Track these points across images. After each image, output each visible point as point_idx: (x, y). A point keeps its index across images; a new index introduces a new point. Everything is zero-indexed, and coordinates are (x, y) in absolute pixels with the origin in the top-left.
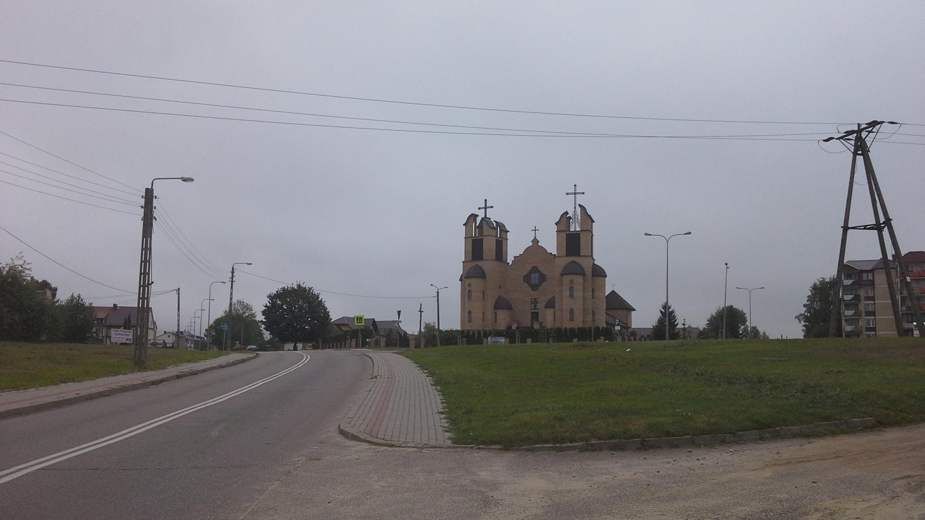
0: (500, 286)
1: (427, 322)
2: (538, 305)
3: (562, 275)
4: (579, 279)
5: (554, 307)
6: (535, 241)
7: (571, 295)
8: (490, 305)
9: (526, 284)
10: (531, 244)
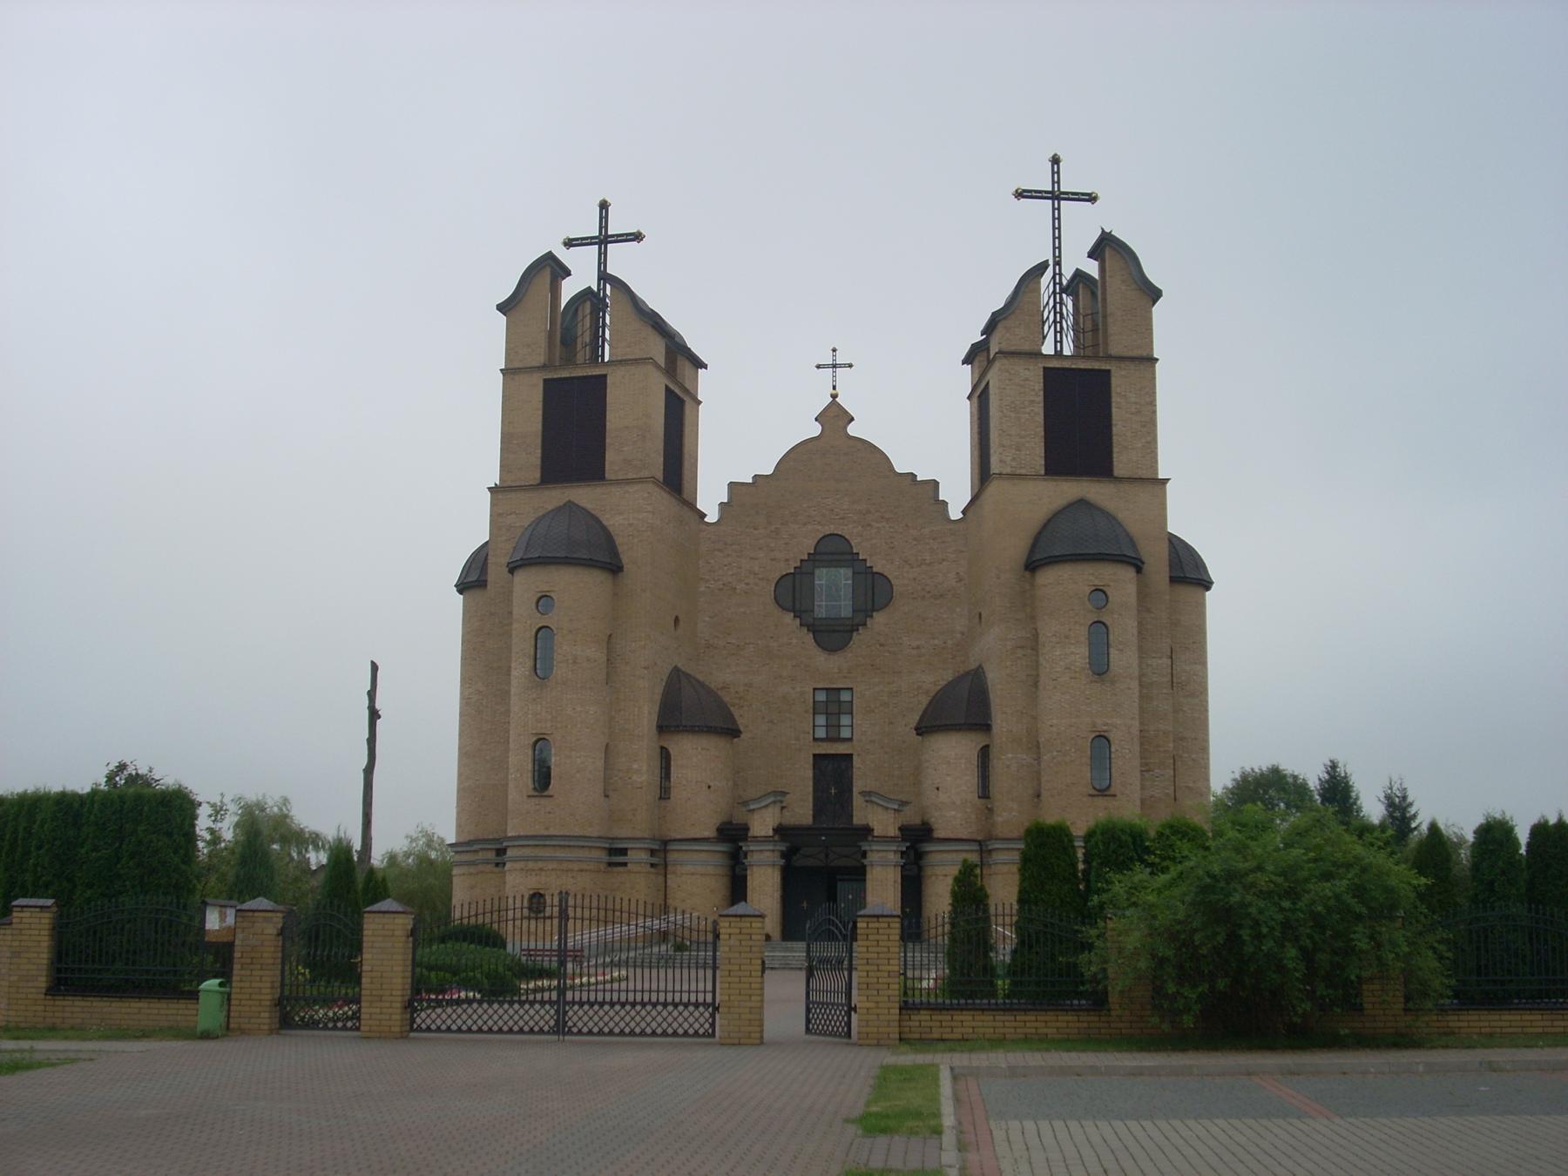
0: (677, 620)
1: (251, 796)
2: (845, 720)
3: (1032, 565)
4: (1121, 582)
5: (986, 727)
6: (835, 416)
7: (1100, 668)
8: (645, 714)
9: (788, 618)
10: (816, 430)
